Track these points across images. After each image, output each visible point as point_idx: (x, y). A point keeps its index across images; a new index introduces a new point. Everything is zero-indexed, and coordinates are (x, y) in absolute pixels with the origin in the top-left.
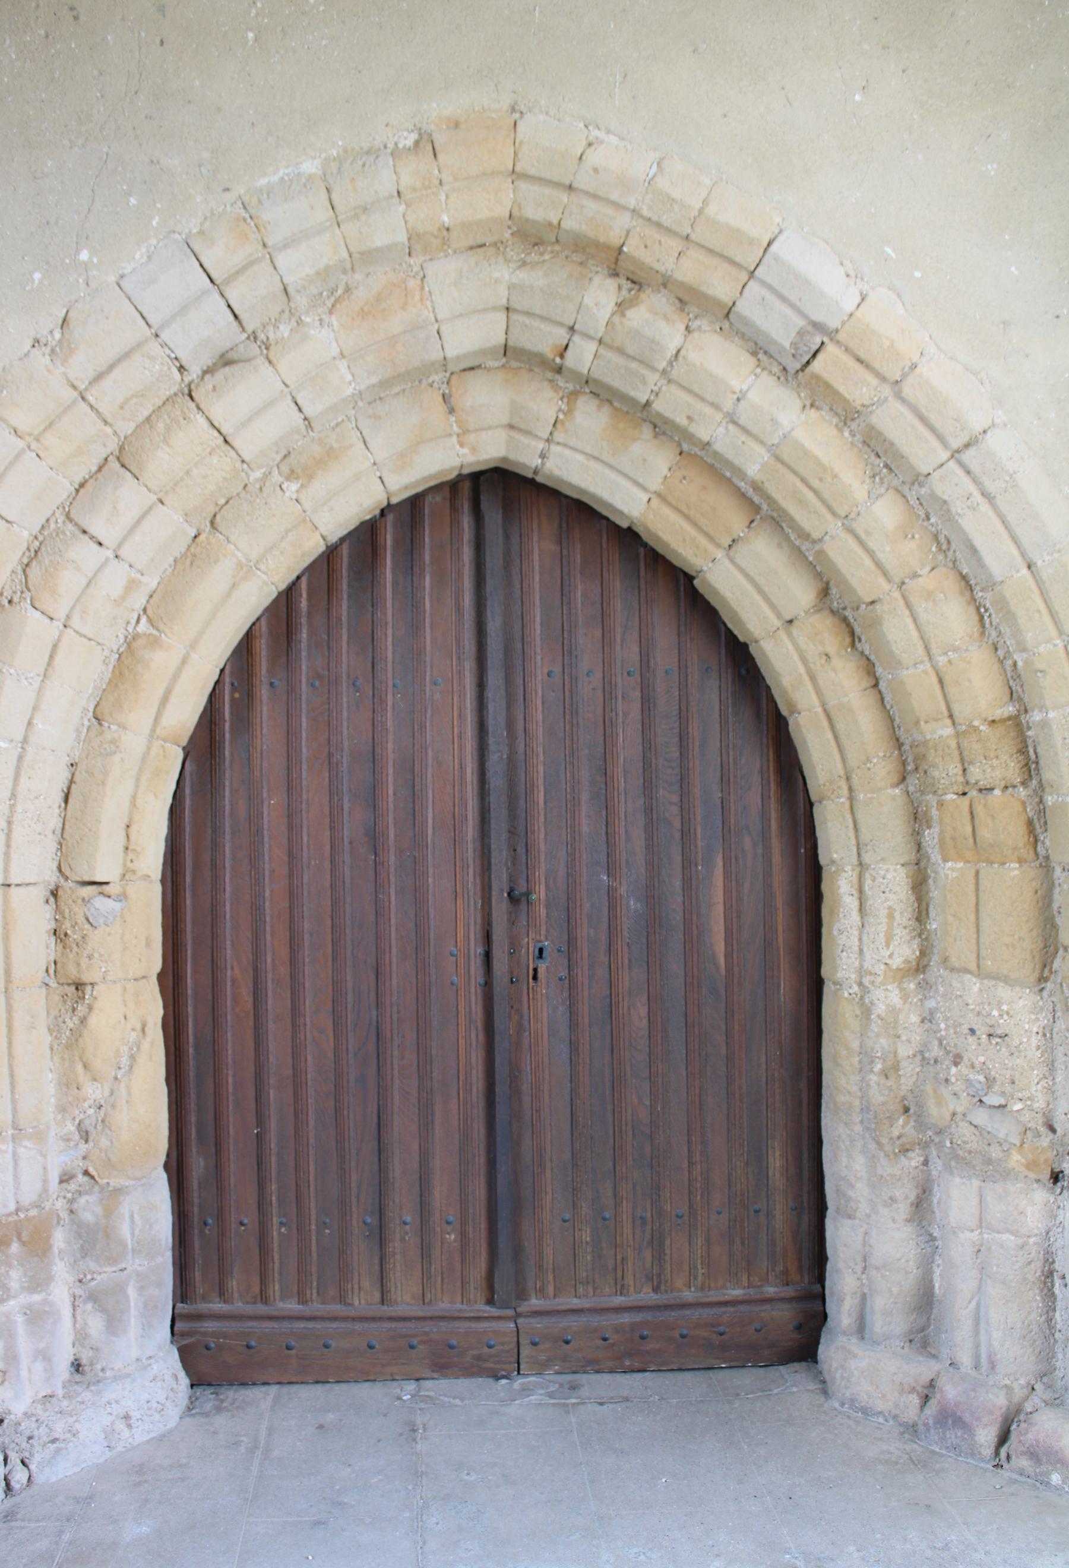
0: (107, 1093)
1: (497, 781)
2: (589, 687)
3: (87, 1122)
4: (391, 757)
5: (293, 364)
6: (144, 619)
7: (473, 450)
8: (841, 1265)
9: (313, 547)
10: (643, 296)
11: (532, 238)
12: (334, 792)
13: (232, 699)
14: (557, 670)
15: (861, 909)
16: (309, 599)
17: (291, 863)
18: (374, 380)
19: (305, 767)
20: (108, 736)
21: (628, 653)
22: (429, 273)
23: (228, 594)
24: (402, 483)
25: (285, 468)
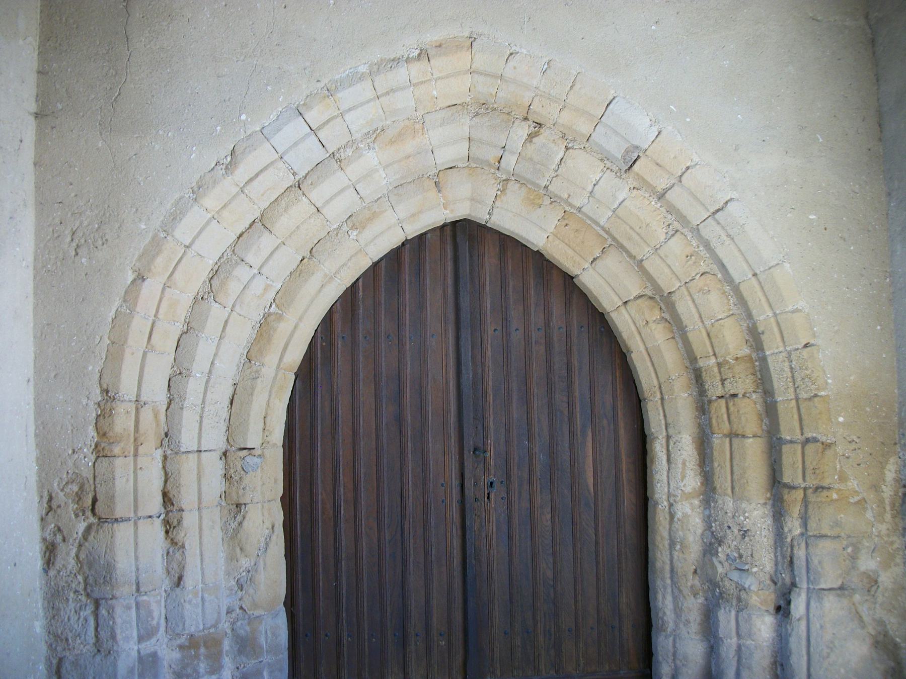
0: (253, 564)
1: (467, 391)
2: (517, 337)
3: (242, 580)
4: (409, 377)
5: (354, 170)
6: (274, 306)
7: (452, 211)
8: (660, 658)
9: (366, 264)
10: (542, 130)
11: (484, 108)
12: (377, 396)
13: (321, 345)
14: (499, 328)
15: (669, 461)
16: (364, 291)
17: (354, 435)
18: (398, 176)
19: (361, 383)
20: (255, 368)
21: (537, 318)
22: (427, 120)
23: (320, 291)
24: (413, 230)
25: (350, 223)
